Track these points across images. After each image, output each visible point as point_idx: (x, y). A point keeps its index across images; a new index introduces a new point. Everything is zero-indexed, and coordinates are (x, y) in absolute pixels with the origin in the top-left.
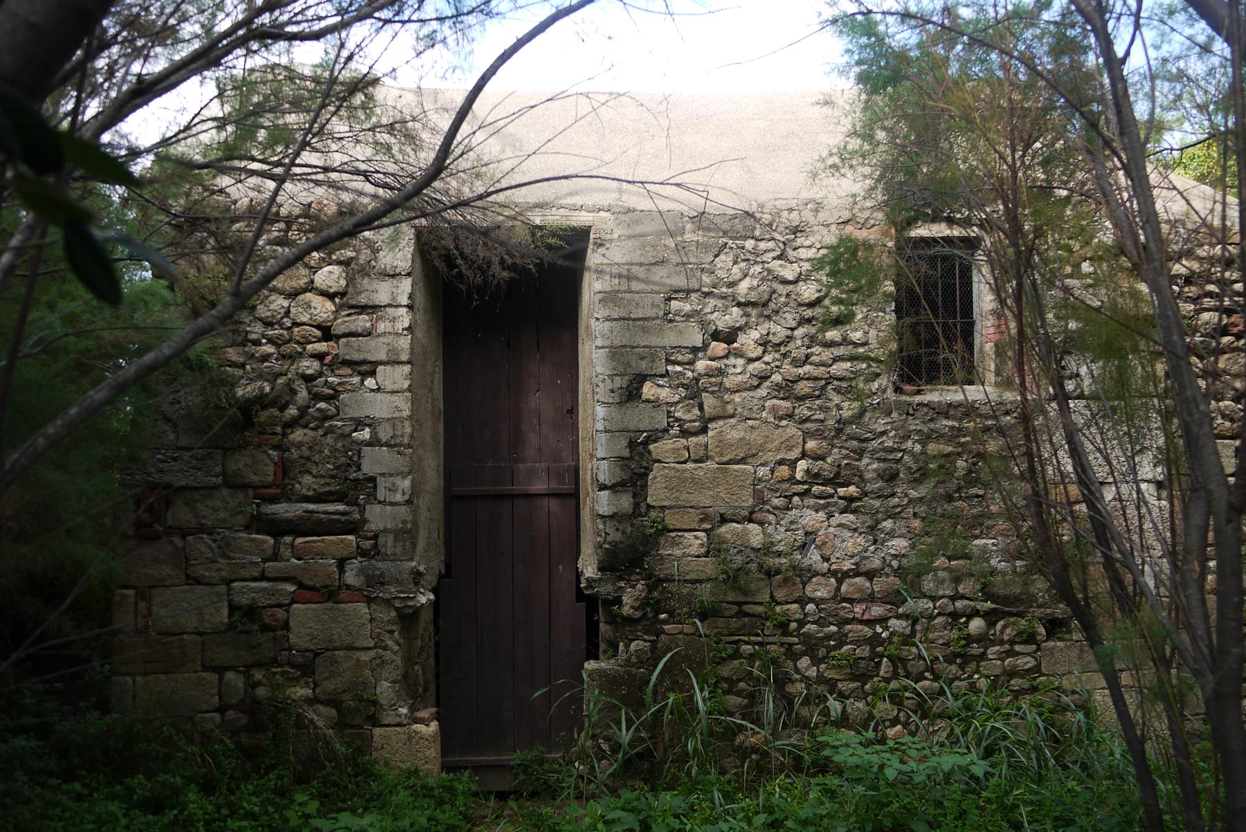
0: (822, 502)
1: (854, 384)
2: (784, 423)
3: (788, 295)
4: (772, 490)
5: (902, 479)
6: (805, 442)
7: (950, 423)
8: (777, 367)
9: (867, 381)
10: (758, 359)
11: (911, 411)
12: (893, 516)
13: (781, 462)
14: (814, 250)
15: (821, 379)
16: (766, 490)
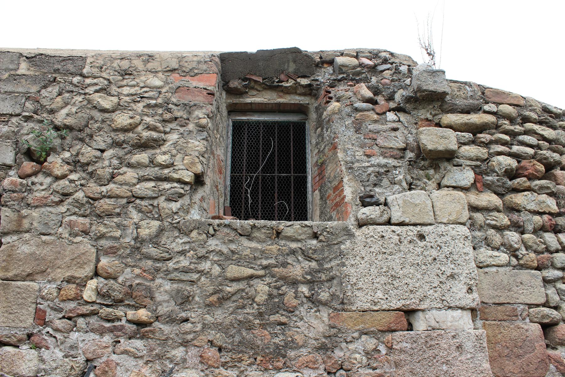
0: (108, 325)
1: (155, 203)
2: (79, 239)
3: (103, 121)
4: (55, 310)
5: (197, 303)
6: (98, 261)
7: (254, 245)
8: (81, 185)
9: (169, 200)
10: (64, 177)
11: (211, 231)
12: (185, 344)
13: (69, 281)
14: (137, 88)
15: (122, 197)
16: (48, 310)
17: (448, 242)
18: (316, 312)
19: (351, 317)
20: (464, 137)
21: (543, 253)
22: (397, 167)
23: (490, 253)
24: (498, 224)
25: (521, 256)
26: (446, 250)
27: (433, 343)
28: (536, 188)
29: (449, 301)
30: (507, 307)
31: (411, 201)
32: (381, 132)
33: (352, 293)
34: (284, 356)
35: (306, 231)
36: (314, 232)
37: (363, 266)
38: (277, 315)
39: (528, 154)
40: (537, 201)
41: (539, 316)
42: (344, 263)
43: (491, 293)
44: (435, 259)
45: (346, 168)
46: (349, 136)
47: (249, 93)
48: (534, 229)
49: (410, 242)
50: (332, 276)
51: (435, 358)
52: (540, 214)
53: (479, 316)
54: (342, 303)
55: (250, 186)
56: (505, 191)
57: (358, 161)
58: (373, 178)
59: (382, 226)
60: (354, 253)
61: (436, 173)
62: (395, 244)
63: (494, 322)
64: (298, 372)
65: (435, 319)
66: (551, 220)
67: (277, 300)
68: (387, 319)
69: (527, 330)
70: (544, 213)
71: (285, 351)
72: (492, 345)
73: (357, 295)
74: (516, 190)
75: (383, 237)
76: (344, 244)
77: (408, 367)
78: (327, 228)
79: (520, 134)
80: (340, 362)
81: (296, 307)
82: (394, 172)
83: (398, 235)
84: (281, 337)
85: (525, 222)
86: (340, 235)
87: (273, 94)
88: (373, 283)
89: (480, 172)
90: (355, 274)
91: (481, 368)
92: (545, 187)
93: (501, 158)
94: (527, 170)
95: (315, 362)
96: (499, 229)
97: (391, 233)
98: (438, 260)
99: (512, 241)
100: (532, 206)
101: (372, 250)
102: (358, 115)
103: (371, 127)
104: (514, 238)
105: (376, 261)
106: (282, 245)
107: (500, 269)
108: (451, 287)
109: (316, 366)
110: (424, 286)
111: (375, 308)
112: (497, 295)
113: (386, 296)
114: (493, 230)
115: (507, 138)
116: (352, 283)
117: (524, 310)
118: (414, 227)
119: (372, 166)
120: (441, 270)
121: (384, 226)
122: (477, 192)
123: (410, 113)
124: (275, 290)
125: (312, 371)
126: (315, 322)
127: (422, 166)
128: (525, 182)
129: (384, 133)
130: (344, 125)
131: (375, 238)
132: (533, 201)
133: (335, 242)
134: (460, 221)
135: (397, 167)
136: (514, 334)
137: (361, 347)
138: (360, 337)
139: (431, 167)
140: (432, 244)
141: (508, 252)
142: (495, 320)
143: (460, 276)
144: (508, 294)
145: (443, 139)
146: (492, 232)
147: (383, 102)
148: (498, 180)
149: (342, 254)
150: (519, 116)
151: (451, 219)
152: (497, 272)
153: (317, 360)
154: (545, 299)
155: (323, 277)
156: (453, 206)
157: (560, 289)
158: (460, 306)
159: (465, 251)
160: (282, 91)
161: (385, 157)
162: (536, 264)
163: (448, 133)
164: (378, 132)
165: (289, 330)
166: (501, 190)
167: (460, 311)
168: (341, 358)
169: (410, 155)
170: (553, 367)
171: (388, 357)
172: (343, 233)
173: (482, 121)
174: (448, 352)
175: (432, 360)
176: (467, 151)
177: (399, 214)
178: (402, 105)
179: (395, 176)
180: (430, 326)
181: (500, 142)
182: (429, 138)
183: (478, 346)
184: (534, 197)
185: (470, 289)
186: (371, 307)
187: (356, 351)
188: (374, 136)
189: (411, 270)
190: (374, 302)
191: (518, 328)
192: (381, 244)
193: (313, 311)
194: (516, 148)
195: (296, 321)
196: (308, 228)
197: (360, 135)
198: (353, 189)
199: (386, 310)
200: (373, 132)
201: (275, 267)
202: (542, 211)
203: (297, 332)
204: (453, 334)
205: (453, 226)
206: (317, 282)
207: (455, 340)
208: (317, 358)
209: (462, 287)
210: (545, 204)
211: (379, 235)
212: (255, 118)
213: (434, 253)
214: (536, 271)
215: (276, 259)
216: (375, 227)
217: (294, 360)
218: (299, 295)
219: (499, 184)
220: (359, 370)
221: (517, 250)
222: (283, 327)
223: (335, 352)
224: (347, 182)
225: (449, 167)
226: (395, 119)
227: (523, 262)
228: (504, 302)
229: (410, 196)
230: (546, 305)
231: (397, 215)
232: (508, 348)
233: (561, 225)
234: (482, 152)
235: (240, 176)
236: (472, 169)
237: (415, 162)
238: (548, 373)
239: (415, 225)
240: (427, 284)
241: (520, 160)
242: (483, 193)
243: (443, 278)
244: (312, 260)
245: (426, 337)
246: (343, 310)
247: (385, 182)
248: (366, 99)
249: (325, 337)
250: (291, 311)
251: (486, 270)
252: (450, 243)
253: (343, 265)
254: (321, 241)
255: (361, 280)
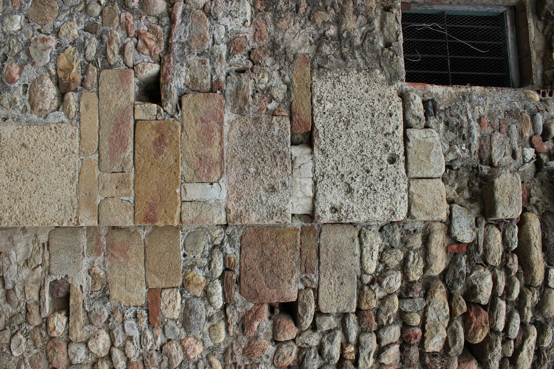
17: (387, 189)
18: (310, 42)
19: (305, 75)
20: (512, 236)
21: (377, 320)
22: (469, 149)
23: (376, 248)
24: (409, 264)
25: (373, 288)
26: (379, 186)
27: (278, 159)
28: (454, 326)
29: (323, 182)
30: (315, 261)
31: (433, 151)
32: (509, 139)
33: (329, 78)
34: (266, 10)
35: (392, 36)
36: (391, 43)
37: (359, 91)
38: (306, 5)
39: (496, 320)
40: (438, 322)
41: (305, 301)
42: (361, 71)
43: (330, 243)
44: (368, 172)
45: (463, 92)
46: (500, 103)
47: (539, 22)
48: (405, 312)
49: (386, 146)
50: (347, 57)
51: (263, 160)
52: (423, 326)
53: (305, 224)
54: (319, 67)
55: (434, 28)
56: (448, 282)
57: (473, 108)
58: (455, 121)
59: (402, 116)
60: (372, 83)
61: (465, 199)
62: (383, 128)
63: (299, 242)
64: (251, 23)
65: (303, 164)
66: (416, 338)
67: (320, 4)
68: (303, 111)
69: (289, 282)
70: (424, 331)
71: (271, 10)
72: (275, 237)
73: (327, 82)
74: (450, 297)
75: (391, 115)
76: (381, 73)
77: (254, 130)
78: (397, 56)
79: (522, 316)
80: (260, 61)
81: (314, 22)
82: (464, 145)
83: (393, 133)
84: (284, 8)
85: (412, 300)
86: (390, 69)
87: (540, 46)
88: (341, 100)
89: (470, 251)
90: (350, 82)
91: (251, 210)
92: (456, 338)
93: (489, 280)
94: (476, 316)
95: (260, 38)
96: (404, 266)
97: (395, 125)
98: (368, 175)
99: (390, 279)
100: (431, 316)
101: (376, 102)
102: (526, 115)
103: (514, 127)
104: (393, 281)
105: (364, 105)
106: (377, 11)
107: (357, 258)
108: (337, 186)
109: (257, 39)
110: (338, 156)
111: (314, 101)
112: (328, 250)
113: (327, 113)
114: (402, 258)
115: (516, 294)
116: (340, 78)
117: (312, 281)
118: (403, 153)
119: (469, 121)
120: (356, 177)
121: (402, 118)
122: (446, 245)
123: (535, 177)
124: (331, 3)
125: (252, 35)
126: (299, 41)
127: (473, 184)
128: (461, 308)
129: (508, 142)
130: (513, 100)
131: (388, 107)
132: (438, 317)
133: (382, 64)
134: (412, 207)
135: (469, 149)
136: (287, 266)
137: (274, 83)
138: (285, 83)
139: (473, 195)
140: (384, 170)
141: (377, 274)
142: (301, 243)
143: (350, 199)
144: (330, 265)
145: (508, 199)
146: (401, 256)
147: (546, 147)
148: (461, 272)
149: (370, 70)
150: (546, 319)
151: (415, 196)
152: (355, 255)
153: (263, 40)
154: (324, 312)
155: (345, 50)
156: (429, 201)
157: (336, 334)
158: (317, 195)
159: (378, 208)
160: (545, 55)
161: (480, 139)
162: (364, 307)
163: (517, 207)
164: (508, 135)
165: (292, 16)
166: (450, 277)
167: (312, 194)
168: (265, 62)
169: (485, 169)
170: (251, 306)
171: (265, 110)
172: (393, 72)
173: (535, 262)
174: (268, 176)
175: (260, 157)
176: (495, 237)
177: (417, 136)
178: (545, 167)
179: (459, 145)
180: (295, 158)
181: (510, 285)
182: (508, 182)
183: (274, 210)
184: (443, 320)
185: (336, 210)
186: (316, 97)
187: (271, 78)
188: (503, 130)
189: (355, 142)
190: (320, 100)
191: (292, 272)
192: (383, 112)
193: (311, 38)
194: (502, 304)
195: (300, 22)
196: (395, 38)
197: (503, 114)
198: (441, 97)
199: (312, 112)
200: (509, 129)
201: (354, 4)
202: (426, 328)
203: (290, 22)
204: (287, 182)
205: (406, 196)
206: (341, 43)
207: (280, 185)
208: (265, 40)
209: (338, 201)
210: (434, 333)
211: (393, 111)
212: (510, 35)
213: (375, 172)
214: (355, 307)
215: (362, 5)
216: (401, 109)
217: (263, 19)
218: (326, 26)
219: (458, 273)
220: (252, 80)
221: (380, 284)
222: (294, 10)
223: (270, 58)
224: (448, 91)
225: (474, 212)
226: (526, 157)
227: (365, 289)
228: (321, 258)
229: (438, 152)
230: (318, 312)
231: (415, 134)
232: (271, 255)
233: (409, 351)
234: (496, 258)
235: (444, 19)
236: (474, 241)
237: (477, 175)
238: (245, 300)
239: (406, 154)
240: (341, 159)
241: (488, 310)
242: (445, 253)
243: (347, 179)
244: (362, 40)
245: (284, 153)
246: (312, 68)
247: (452, 136)
248: (547, 127)
249: (285, 49)
250: (310, 18)
251: (357, 241)
252: (387, 191)
253: (359, 71)
254: (383, 50)
255: (344, 87)
